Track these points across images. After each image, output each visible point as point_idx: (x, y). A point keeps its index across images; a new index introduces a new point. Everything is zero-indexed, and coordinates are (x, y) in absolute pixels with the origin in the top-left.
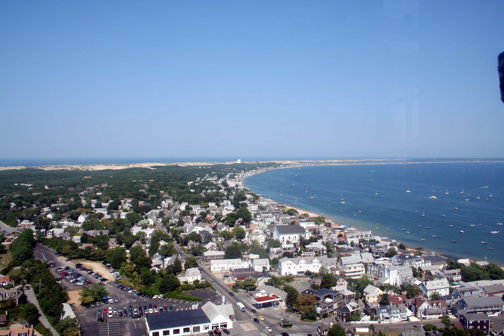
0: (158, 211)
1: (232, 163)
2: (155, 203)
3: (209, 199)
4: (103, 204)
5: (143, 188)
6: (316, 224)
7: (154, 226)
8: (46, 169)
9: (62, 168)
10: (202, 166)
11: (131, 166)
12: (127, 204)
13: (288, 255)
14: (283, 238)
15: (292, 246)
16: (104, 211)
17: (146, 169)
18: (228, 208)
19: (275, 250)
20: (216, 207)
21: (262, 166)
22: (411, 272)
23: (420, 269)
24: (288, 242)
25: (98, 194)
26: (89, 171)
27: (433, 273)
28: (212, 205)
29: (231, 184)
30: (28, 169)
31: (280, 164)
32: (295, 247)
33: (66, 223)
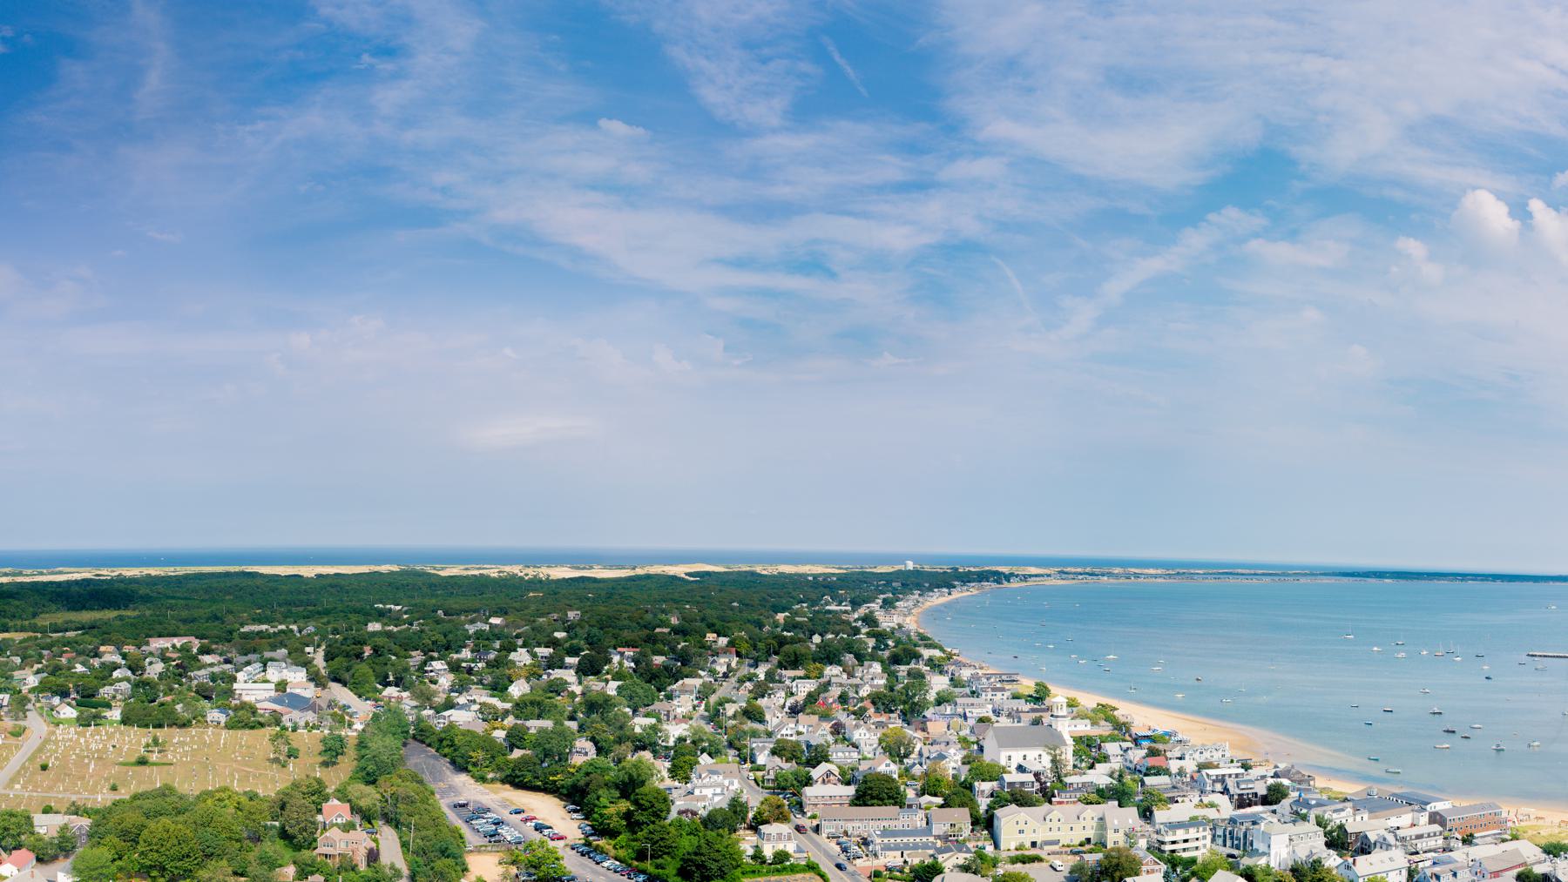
0: (697, 682)
1: (890, 570)
2: (685, 663)
3: (829, 656)
4: (569, 660)
5: (663, 624)
6: (1093, 724)
7: (687, 718)
8: (443, 574)
9: (476, 572)
10: (815, 577)
11: (640, 571)
12: (623, 659)
13: (1020, 798)
14: (1010, 758)
15: (1030, 777)
16: (569, 676)
17: (674, 578)
18: (873, 677)
19: (987, 786)
20: (845, 676)
21: (966, 578)
22: (1321, 840)
23: (1341, 827)
24: (1021, 769)
25: (557, 634)
26: (541, 581)
27: (1372, 837)
28: (832, 671)
29: (887, 622)
30: (402, 573)
31: (1012, 574)
32: (1038, 780)
33: (482, 696)
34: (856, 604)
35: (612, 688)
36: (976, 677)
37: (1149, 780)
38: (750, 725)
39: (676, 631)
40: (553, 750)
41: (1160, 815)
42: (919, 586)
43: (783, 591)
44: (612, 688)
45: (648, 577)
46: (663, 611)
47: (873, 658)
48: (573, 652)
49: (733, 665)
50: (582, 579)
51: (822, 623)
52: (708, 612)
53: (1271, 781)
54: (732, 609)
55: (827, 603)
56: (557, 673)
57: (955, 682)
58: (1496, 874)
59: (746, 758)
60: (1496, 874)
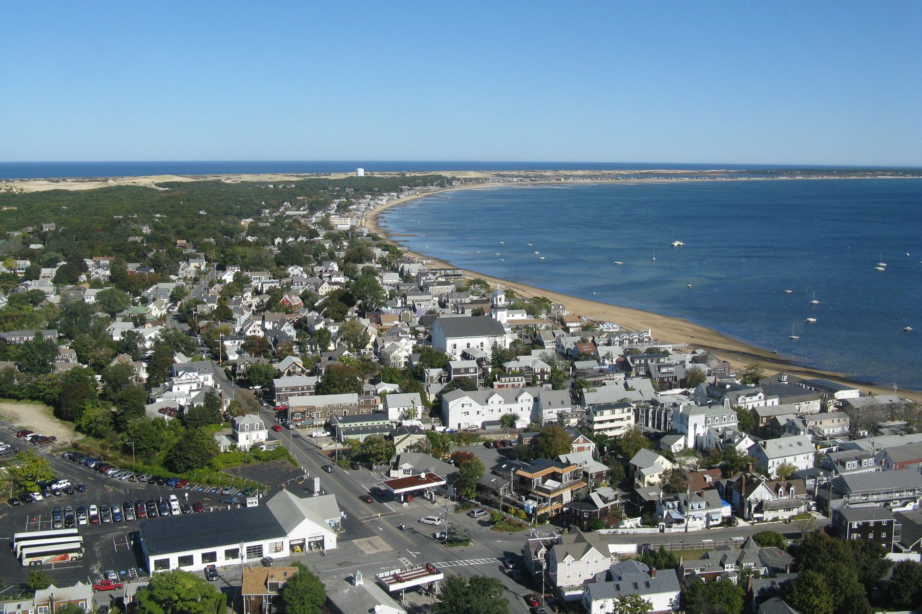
3: (289, 257)
4: (45, 271)
7: (162, 319)
10: (276, 184)
11: (111, 183)
12: (99, 269)
13: (466, 385)
14: (455, 346)
15: (473, 364)
17: (145, 189)
19: (434, 373)
21: (412, 183)
22: (734, 423)
25: (32, 246)
26: (14, 195)
27: (782, 421)
28: (295, 271)
31: (454, 178)
34: (312, 210)
35: (90, 297)
36: (421, 274)
37: (579, 365)
38: (221, 325)
39: (148, 238)
40: (37, 358)
41: (590, 397)
42: (370, 191)
43: (249, 199)
44: (90, 297)
45: (119, 188)
46: (135, 221)
47: (332, 257)
48: (50, 264)
49: (203, 268)
50: (57, 192)
51: (284, 227)
52: (179, 220)
53: (689, 366)
54: (200, 216)
55: (286, 209)
56: (33, 285)
57: (406, 278)
58: (902, 466)
59: (218, 355)
60: (902, 466)
